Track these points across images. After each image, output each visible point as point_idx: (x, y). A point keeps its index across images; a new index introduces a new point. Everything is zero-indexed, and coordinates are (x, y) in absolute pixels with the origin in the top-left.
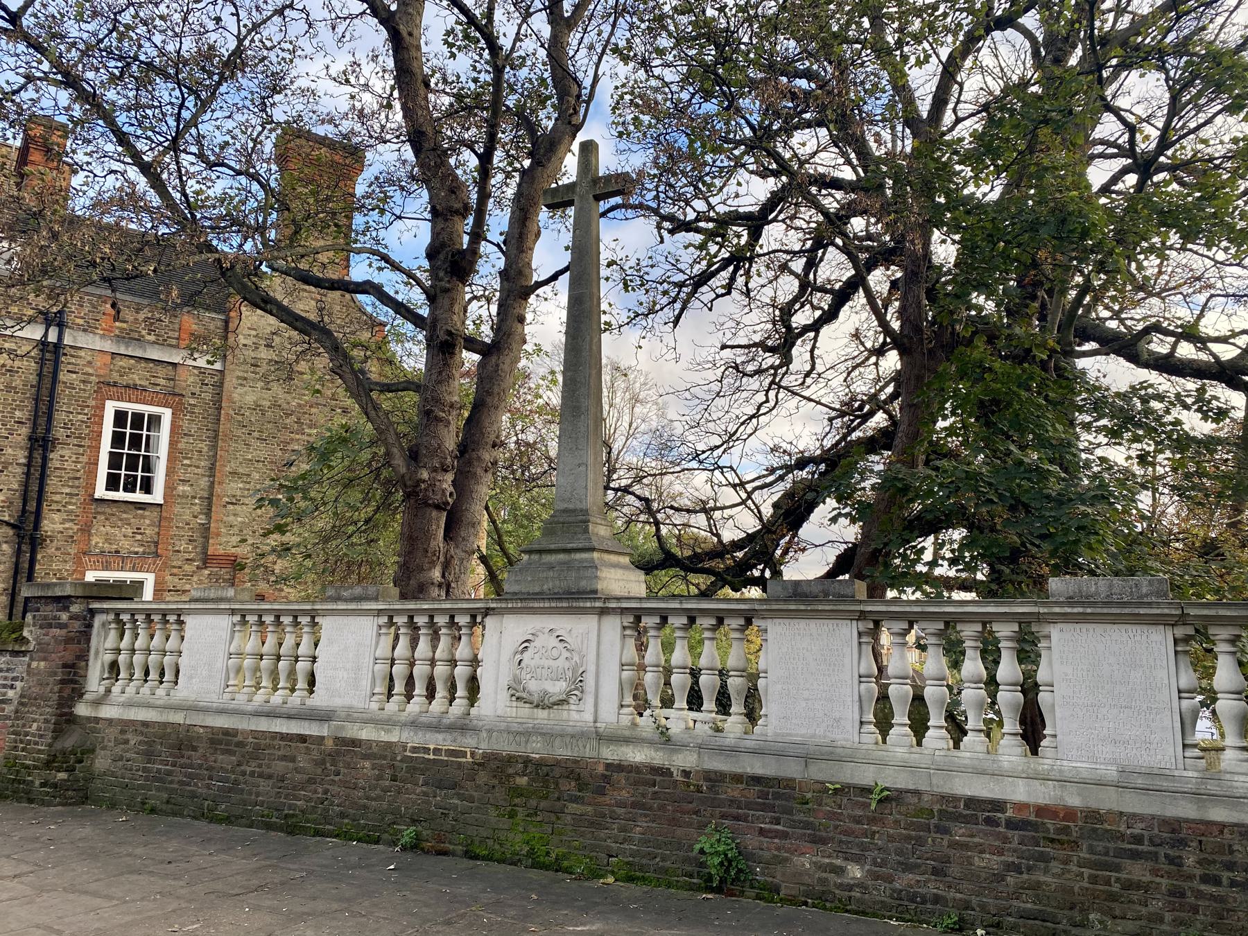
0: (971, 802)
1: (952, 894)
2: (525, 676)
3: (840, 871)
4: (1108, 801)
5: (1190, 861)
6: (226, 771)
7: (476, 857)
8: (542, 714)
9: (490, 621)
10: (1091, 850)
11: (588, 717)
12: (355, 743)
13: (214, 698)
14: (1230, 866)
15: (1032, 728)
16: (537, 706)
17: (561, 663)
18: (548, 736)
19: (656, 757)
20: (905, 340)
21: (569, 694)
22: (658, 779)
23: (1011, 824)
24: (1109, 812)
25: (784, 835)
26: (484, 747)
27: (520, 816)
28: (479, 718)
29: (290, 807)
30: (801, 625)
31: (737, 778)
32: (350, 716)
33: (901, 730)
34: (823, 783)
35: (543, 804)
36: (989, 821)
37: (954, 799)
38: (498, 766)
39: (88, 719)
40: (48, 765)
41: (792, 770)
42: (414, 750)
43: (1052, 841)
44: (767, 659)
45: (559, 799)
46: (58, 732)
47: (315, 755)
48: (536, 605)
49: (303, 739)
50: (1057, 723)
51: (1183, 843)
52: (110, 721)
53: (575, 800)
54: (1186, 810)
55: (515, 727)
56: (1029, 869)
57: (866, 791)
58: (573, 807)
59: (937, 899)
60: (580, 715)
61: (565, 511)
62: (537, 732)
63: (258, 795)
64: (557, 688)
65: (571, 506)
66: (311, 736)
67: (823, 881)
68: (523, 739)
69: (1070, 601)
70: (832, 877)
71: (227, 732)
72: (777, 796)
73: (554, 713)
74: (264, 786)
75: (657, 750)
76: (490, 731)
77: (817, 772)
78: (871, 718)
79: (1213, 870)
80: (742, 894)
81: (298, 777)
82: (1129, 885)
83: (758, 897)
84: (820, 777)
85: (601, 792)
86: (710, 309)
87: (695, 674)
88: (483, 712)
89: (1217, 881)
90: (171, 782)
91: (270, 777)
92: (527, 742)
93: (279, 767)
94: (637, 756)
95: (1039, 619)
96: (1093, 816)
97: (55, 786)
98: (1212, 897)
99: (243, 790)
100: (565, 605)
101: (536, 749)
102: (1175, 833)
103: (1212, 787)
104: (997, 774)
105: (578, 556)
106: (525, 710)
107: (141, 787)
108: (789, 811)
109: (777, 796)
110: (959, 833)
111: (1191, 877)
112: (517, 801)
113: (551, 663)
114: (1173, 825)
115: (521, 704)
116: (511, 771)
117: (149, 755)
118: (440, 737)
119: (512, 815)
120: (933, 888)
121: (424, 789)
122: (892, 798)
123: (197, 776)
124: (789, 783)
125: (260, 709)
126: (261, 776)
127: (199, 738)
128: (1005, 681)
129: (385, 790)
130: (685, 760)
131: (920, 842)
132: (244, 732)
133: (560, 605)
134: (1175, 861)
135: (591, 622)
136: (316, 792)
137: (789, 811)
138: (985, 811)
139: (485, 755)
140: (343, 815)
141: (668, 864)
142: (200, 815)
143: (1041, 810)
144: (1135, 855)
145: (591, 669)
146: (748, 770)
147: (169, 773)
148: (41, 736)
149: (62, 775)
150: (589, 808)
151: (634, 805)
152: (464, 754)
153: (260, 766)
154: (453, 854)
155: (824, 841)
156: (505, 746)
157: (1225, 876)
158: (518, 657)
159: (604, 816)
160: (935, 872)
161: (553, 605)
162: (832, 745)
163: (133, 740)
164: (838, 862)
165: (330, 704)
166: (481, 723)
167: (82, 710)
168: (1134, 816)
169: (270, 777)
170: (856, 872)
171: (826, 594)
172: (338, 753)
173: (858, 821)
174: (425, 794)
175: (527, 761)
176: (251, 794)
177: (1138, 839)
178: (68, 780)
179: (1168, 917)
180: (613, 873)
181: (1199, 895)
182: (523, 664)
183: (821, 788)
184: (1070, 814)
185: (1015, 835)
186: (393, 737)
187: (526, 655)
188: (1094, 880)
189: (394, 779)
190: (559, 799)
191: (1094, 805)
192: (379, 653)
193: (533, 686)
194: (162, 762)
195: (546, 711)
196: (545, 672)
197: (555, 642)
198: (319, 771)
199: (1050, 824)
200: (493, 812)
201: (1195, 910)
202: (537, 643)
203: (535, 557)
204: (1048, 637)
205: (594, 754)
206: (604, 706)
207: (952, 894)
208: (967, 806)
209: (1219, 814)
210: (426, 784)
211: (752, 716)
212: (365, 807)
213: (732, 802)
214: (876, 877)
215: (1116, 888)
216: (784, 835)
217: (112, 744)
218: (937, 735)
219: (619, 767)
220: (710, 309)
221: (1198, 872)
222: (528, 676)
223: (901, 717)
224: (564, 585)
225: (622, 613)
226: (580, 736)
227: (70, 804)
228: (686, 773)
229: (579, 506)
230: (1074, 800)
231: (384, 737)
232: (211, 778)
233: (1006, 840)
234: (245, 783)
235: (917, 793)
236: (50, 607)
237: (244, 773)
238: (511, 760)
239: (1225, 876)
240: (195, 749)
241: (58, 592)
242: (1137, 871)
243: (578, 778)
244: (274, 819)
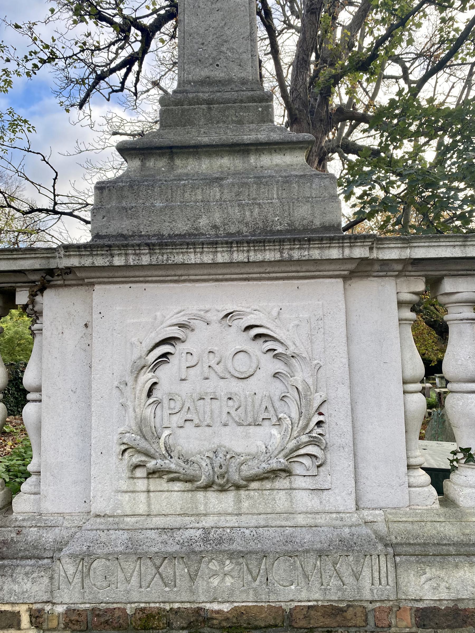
2: (159, 417)
8: (215, 501)
11: (340, 499)
16: (206, 487)
17: (262, 386)
18: (251, 556)
20: (297, 112)
21: (292, 454)
26: (70, 596)
28: (40, 520)
44: (40, 370)
48: (192, 258)
55: (154, 543)
60: (317, 503)
61: (207, 82)
62: (195, 554)
64: (260, 443)
65: (219, 74)
68: (181, 570)
73: (251, 499)
76: (85, 558)
86: (108, 100)
88: (49, 506)
92: (192, 578)
100: (271, 255)
106: (170, 499)
113: (235, 386)
115: (162, 484)
128: (462, 375)
133: (256, 256)
135: (329, 292)
145: (340, 394)
158: (146, 378)
161: (239, 257)
166: (49, 537)
182: (157, 394)
187: (165, 373)
193: (192, 442)
195: (230, 497)
196: (221, 408)
197: (243, 341)
202: (194, 343)
205: (388, 591)
220: (108, 100)
222: (176, 420)
225: (399, 275)
226: (345, 548)
229: (237, 73)
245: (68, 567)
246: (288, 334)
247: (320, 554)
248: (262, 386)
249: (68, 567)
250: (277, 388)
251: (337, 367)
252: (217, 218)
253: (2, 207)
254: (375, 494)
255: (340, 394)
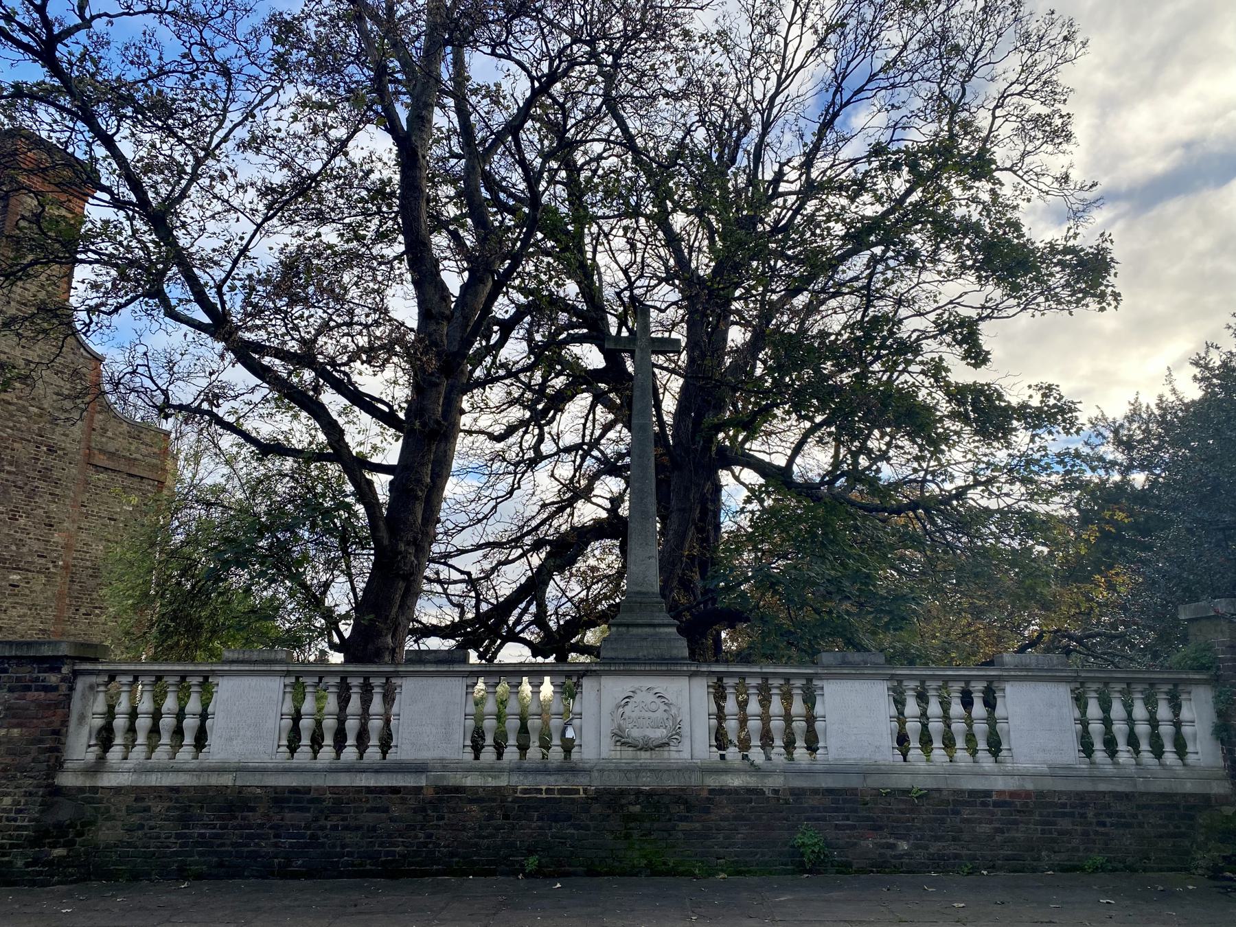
0: (972, 793)
1: (965, 852)
3: (893, 847)
4: (1048, 785)
5: (1090, 814)
6: (299, 827)
7: (598, 874)
8: (644, 756)
9: (587, 683)
10: (1041, 815)
12: (458, 789)
13: (266, 758)
14: (1109, 815)
15: (995, 746)
17: (660, 714)
19: (751, 781)
21: (670, 738)
22: (754, 797)
23: (996, 804)
24: (1049, 791)
25: (853, 827)
27: (635, 837)
29: (388, 854)
30: (857, 685)
31: (815, 791)
32: (445, 766)
33: (915, 753)
34: (878, 789)
35: (656, 825)
36: (984, 804)
37: (962, 791)
38: (611, 799)
39: (81, 790)
40: (35, 842)
41: (854, 782)
42: (525, 791)
43: (1019, 811)
45: (670, 820)
46: (46, 807)
47: (412, 803)
49: (395, 790)
50: (213, 740)
51: (1086, 805)
52: (118, 790)
53: (682, 819)
54: (1086, 786)
55: (625, 767)
56: (1008, 830)
57: (906, 792)
58: (682, 825)
59: (956, 856)
60: (680, 754)
61: (639, 593)
62: (638, 771)
63: (343, 846)
64: (659, 734)
65: (644, 590)
66: (405, 787)
67: (881, 855)
69: (1016, 668)
70: (890, 852)
71: (294, 790)
72: (845, 801)
73: (655, 754)
74: (349, 837)
75: (751, 776)
76: (601, 771)
77: (873, 782)
78: (286, 743)
79: (1103, 819)
80: (826, 871)
81: (393, 826)
82: (1061, 833)
83: (838, 872)
84: (876, 785)
85: (707, 811)
87: (500, 717)
88: (585, 756)
89: (1104, 824)
90: (223, 845)
91: (358, 828)
93: (369, 819)
94: (735, 782)
95: (1000, 678)
96: (1041, 794)
97: (50, 863)
98: (1102, 834)
99: (323, 844)
100: (664, 668)
101: (647, 783)
102: (1082, 800)
103: (1096, 773)
104: (984, 775)
105: (662, 630)
106: (629, 753)
107: (176, 854)
108: (856, 811)
109: (845, 801)
110: (966, 813)
111: (1091, 823)
112: (632, 825)
113: (651, 714)
114: (1080, 795)
116: (623, 801)
117: (185, 819)
118: (552, 779)
119: (627, 837)
120: (952, 849)
121: (539, 824)
122: (926, 795)
123: (259, 836)
124: (853, 791)
125: (281, 765)
126: (346, 828)
127: (257, 798)
129: (497, 828)
130: (776, 782)
131: (943, 821)
132: (318, 789)
134: (1083, 816)
136: (416, 837)
137: (856, 811)
138: (980, 797)
139: (597, 791)
140: (452, 855)
141: (767, 858)
142: (267, 873)
143: (1013, 794)
144: (1064, 815)
145: (686, 719)
146: (824, 785)
147: (216, 836)
148: (19, 811)
149: (59, 852)
150: (697, 825)
151: (735, 818)
152: (577, 792)
153: (343, 819)
154: (575, 874)
155: (880, 828)
156: (617, 782)
157: (1108, 820)
159: (711, 829)
160: (954, 839)
161: (653, 668)
162: (876, 763)
163: (157, 807)
164: (892, 841)
165: (419, 757)
167: (67, 780)
168: (1061, 792)
169: (358, 828)
170: (904, 846)
171: (866, 663)
172: (440, 800)
173: (902, 812)
174: (540, 828)
175: (639, 792)
176: (334, 846)
177: (1064, 805)
178: (68, 856)
179: (1082, 848)
180: (723, 871)
181: (1096, 833)
183: (877, 793)
184: (1028, 794)
185: (998, 811)
186: (503, 782)
188: (1043, 832)
189: (506, 817)
190: (670, 820)
191: (1040, 788)
192: (285, 710)
193: (636, 733)
194: (206, 826)
197: (654, 698)
198: (420, 818)
199: (1018, 802)
200: (609, 837)
201: (1094, 842)
202: (637, 698)
203: (623, 629)
204: (1004, 690)
206: (697, 746)
207: (965, 852)
208: (970, 796)
209: (1102, 787)
210: (540, 819)
211: (812, 747)
212: (476, 845)
213: (813, 808)
214: (917, 847)
215: (1055, 835)
216: (853, 827)
217: (124, 813)
218: (939, 753)
219: (721, 791)
221: (1094, 820)
223: (305, 740)
224: (657, 652)
227: (71, 882)
228: (776, 791)
230: (1029, 786)
231: (491, 782)
232: (277, 836)
233: (993, 814)
234: (326, 837)
235: (939, 790)
236: (29, 668)
237: (323, 828)
238: (622, 792)
239: (1108, 820)
240: (253, 809)
241: (47, 651)
242: (1065, 824)
243: (686, 802)
244: (368, 867)
245: (596, 774)
246: (671, 697)
247: (679, 770)
248: (660, 714)
249: (596, 774)
250: (666, 715)
251: (686, 709)
252: (645, 653)
253: (82, 8)
254: (697, 754)
255: (686, 719)
